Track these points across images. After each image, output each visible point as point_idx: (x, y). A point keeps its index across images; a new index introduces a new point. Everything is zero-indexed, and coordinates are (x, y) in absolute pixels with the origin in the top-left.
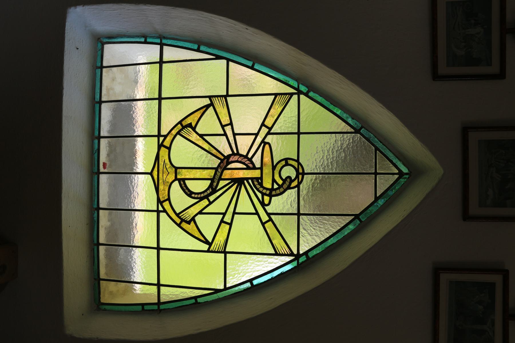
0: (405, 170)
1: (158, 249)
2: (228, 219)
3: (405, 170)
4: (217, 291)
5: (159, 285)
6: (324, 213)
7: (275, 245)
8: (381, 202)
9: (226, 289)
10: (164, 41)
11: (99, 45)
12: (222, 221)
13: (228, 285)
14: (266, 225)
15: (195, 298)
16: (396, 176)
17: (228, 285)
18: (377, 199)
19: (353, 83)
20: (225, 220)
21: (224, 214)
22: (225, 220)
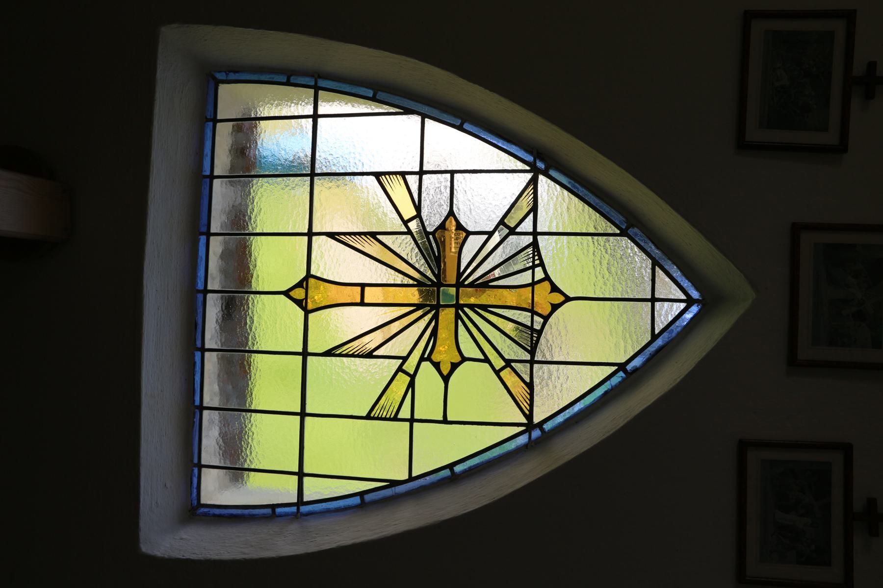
0: (695, 294)
1: (303, 414)
2: (410, 366)
3: (695, 294)
4: (393, 483)
5: (301, 474)
6: (225, 412)
7: (517, 398)
8: (659, 342)
9: (411, 479)
10: (322, 83)
11: (212, 84)
12: (400, 369)
13: (414, 474)
14: (502, 374)
15: (362, 494)
16: (682, 306)
17: (414, 474)
18: (654, 337)
19: (606, 438)
20: (404, 367)
21: (405, 359)
22: (404, 367)
